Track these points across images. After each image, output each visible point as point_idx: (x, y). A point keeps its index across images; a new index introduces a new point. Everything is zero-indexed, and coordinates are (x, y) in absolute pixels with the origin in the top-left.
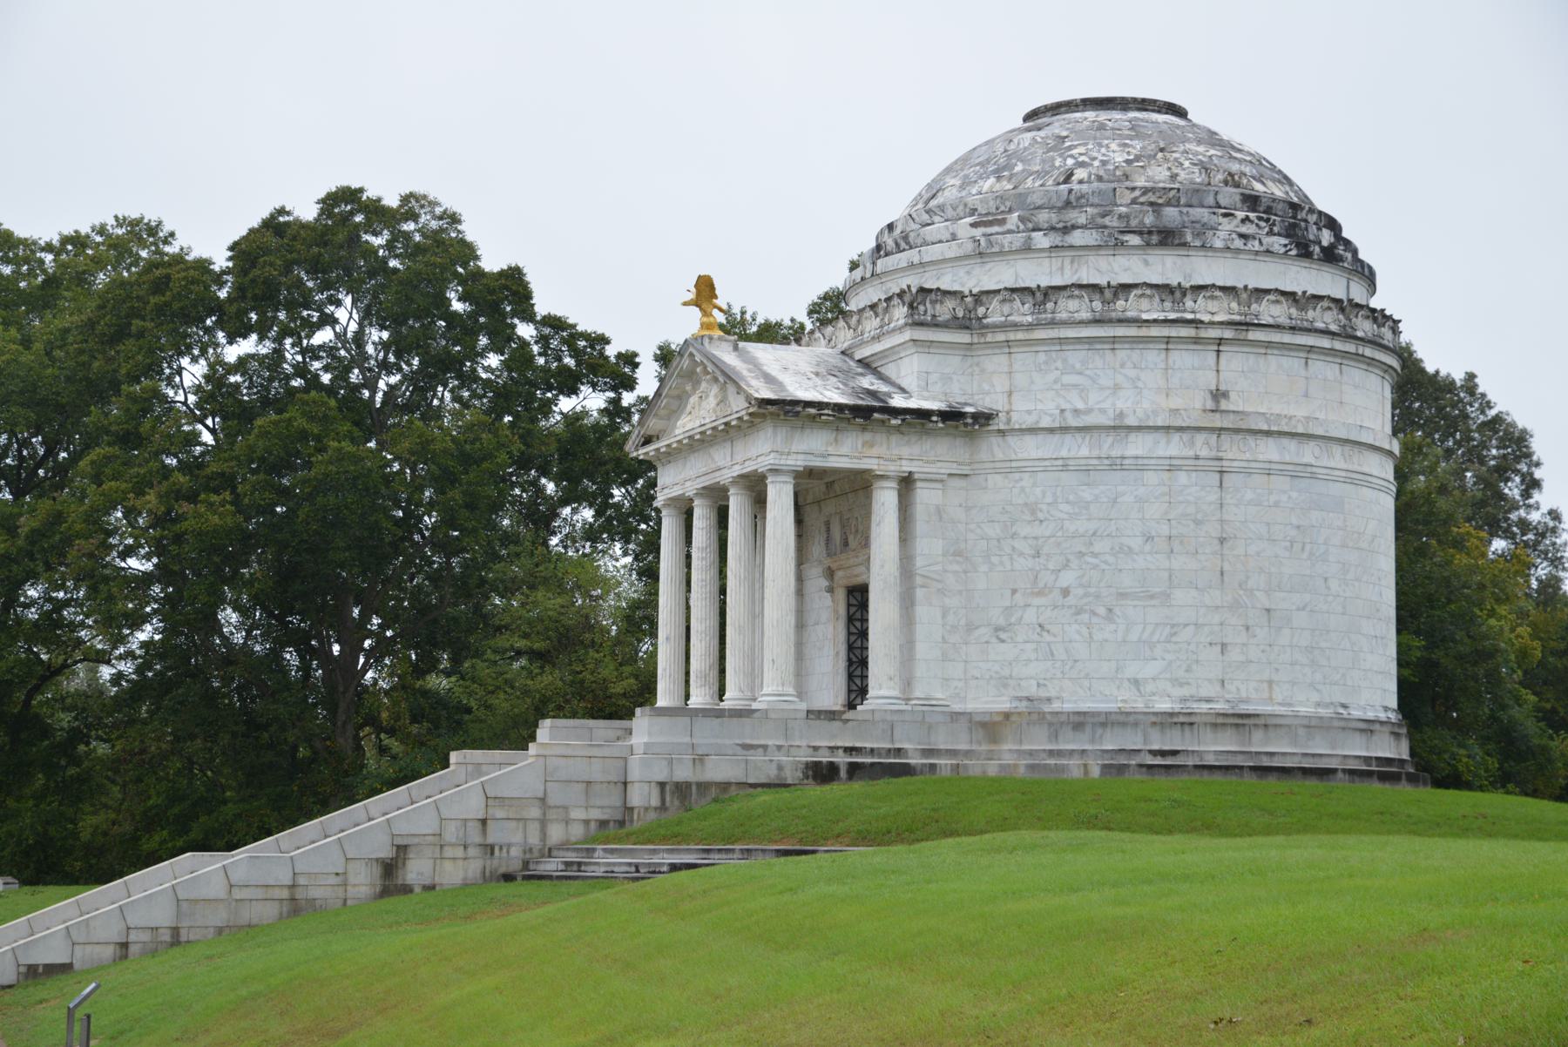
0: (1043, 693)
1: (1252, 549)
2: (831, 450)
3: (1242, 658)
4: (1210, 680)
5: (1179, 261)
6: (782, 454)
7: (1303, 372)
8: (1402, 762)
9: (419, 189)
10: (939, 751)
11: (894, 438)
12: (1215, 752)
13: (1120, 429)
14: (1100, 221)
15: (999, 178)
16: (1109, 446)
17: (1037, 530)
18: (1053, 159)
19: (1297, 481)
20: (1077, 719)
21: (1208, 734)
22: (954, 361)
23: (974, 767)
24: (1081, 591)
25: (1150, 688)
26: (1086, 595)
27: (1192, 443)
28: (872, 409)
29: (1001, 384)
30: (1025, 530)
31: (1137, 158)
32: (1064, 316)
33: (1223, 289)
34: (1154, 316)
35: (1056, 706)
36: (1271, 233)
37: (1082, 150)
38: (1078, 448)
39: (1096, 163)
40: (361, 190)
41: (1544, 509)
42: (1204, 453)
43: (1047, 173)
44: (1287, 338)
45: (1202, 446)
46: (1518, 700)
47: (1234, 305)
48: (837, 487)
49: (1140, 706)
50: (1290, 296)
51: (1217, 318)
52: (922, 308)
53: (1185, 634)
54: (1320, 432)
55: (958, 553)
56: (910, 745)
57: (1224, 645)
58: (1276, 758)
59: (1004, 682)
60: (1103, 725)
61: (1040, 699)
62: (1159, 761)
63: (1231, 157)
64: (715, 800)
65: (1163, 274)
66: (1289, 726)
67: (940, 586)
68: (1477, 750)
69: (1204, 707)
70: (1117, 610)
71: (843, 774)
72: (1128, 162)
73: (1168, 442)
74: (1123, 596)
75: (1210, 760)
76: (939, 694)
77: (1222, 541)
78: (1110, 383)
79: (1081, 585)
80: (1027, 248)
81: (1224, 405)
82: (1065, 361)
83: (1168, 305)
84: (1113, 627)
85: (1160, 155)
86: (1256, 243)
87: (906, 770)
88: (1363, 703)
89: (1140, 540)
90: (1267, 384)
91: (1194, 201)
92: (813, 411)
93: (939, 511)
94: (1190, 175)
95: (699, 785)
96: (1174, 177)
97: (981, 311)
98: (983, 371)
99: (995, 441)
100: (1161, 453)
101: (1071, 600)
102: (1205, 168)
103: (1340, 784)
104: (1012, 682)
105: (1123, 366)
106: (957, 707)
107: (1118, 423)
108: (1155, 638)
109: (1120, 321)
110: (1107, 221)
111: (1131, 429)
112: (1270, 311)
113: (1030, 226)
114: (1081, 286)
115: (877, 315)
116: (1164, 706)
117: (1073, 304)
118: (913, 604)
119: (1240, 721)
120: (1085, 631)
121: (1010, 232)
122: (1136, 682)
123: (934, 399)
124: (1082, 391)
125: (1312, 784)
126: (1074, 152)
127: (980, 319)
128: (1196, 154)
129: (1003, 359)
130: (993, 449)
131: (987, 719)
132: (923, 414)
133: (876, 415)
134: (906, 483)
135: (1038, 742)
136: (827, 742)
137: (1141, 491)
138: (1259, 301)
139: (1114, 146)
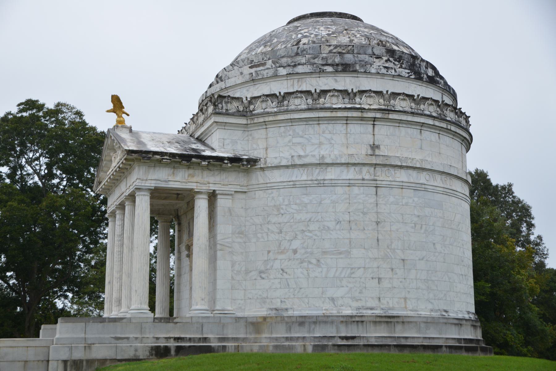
0: (284, 306)
1: (394, 228)
3: (390, 286)
4: (372, 298)
5: (353, 80)
6: (143, 180)
7: (419, 137)
8: (478, 341)
9: (62, 101)
10: (228, 338)
11: (206, 173)
13: (322, 165)
14: (312, 61)
15: (265, 46)
18: (292, 35)
19: (417, 192)
21: (372, 327)
22: (238, 134)
23: (247, 347)
24: (303, 251)
25: (340, 302)
26: (306, 253)
27: (361, 172)
28: (191, 156)
29: (262, 144)
30: (274, 219)
31: (333, 33)
32: (293, 107)
33: (375, 92)
34: (340, 106)
35: (290, 313)
36: (401, 67)
37: (306, 30)
38: (301, 176)
39: (312, 36)
40: (37, 101)
41: (536, 235)
42: (367, 177)
43: (288, 41)
44: (410, 118)
45: (366, 173)
46: (530, 309)
47: (381, 101)
49: (335, 312)
50: (411, 97)
51: (372, 107)
52: (220, 106)
53: (359, 273)
54: (429, 167)
55: (241, 233)
56: (212, 336)
57: (379, 279)
58: (409, 340)
60: (315, 323)
61: (282, 309)
62: (344, 342)
63: (381, 34)
65: (345, 86)
66: (416, 322)
67: (230, 250)
68: (515, 332)
69: (370, 312)
70: (322, 261)
71: (173, 352)
72: (328, 35)
73: (348, 172)
74: (324, 253)
75: (373, 342)
77: (378, 223)
78: (317, 141)
79: (303, 248)
80: (276, 76)
81: (377, 152)
82: (294, 131)
83: (347, 100)
84: (320, 270)
85: (345, 32)
86: (393, 71)
87: (209, 350)
88: (456, 309)
90: (401, 142)
91: (361, 52)
92: (158, 157)
94: (359, 40)
95: (88, 361)
96: (351, 41)
97: (252, 107)
98: (253, 138)
99: (259, 173)
100: (344, 177)
101: (298, 256)
102: (368, 38)
103: (445, 353)
104: (268, 301)
105: (324, 132)
106: (240, 314)
107: (321, 162)
108: (342, 276)
109: (321, 109)
110: (316, 61)
111: (328, 165)
112: (400, 104)
113: (278, 65)
114: (301, 92)
115: (203, 114)
116: (348, 312)
117: (297, 101)
119: (389, 320)
120: (305, 272)
121: (268, 69)
122: (333, 299)
123: (227, 152)
125: (429, 354)
126: (302, 32)
127: (251, 111)
128: (364, 32)
129: (263, 132)
130: (258, 178)
131: (255, 320)
132: (220, 159)
133: (193, 159)
134: (212, 197)
135: (281, 333)
136: (164, 335)
137: (334, 197)
138: (394, 99)
139: (322, 28)
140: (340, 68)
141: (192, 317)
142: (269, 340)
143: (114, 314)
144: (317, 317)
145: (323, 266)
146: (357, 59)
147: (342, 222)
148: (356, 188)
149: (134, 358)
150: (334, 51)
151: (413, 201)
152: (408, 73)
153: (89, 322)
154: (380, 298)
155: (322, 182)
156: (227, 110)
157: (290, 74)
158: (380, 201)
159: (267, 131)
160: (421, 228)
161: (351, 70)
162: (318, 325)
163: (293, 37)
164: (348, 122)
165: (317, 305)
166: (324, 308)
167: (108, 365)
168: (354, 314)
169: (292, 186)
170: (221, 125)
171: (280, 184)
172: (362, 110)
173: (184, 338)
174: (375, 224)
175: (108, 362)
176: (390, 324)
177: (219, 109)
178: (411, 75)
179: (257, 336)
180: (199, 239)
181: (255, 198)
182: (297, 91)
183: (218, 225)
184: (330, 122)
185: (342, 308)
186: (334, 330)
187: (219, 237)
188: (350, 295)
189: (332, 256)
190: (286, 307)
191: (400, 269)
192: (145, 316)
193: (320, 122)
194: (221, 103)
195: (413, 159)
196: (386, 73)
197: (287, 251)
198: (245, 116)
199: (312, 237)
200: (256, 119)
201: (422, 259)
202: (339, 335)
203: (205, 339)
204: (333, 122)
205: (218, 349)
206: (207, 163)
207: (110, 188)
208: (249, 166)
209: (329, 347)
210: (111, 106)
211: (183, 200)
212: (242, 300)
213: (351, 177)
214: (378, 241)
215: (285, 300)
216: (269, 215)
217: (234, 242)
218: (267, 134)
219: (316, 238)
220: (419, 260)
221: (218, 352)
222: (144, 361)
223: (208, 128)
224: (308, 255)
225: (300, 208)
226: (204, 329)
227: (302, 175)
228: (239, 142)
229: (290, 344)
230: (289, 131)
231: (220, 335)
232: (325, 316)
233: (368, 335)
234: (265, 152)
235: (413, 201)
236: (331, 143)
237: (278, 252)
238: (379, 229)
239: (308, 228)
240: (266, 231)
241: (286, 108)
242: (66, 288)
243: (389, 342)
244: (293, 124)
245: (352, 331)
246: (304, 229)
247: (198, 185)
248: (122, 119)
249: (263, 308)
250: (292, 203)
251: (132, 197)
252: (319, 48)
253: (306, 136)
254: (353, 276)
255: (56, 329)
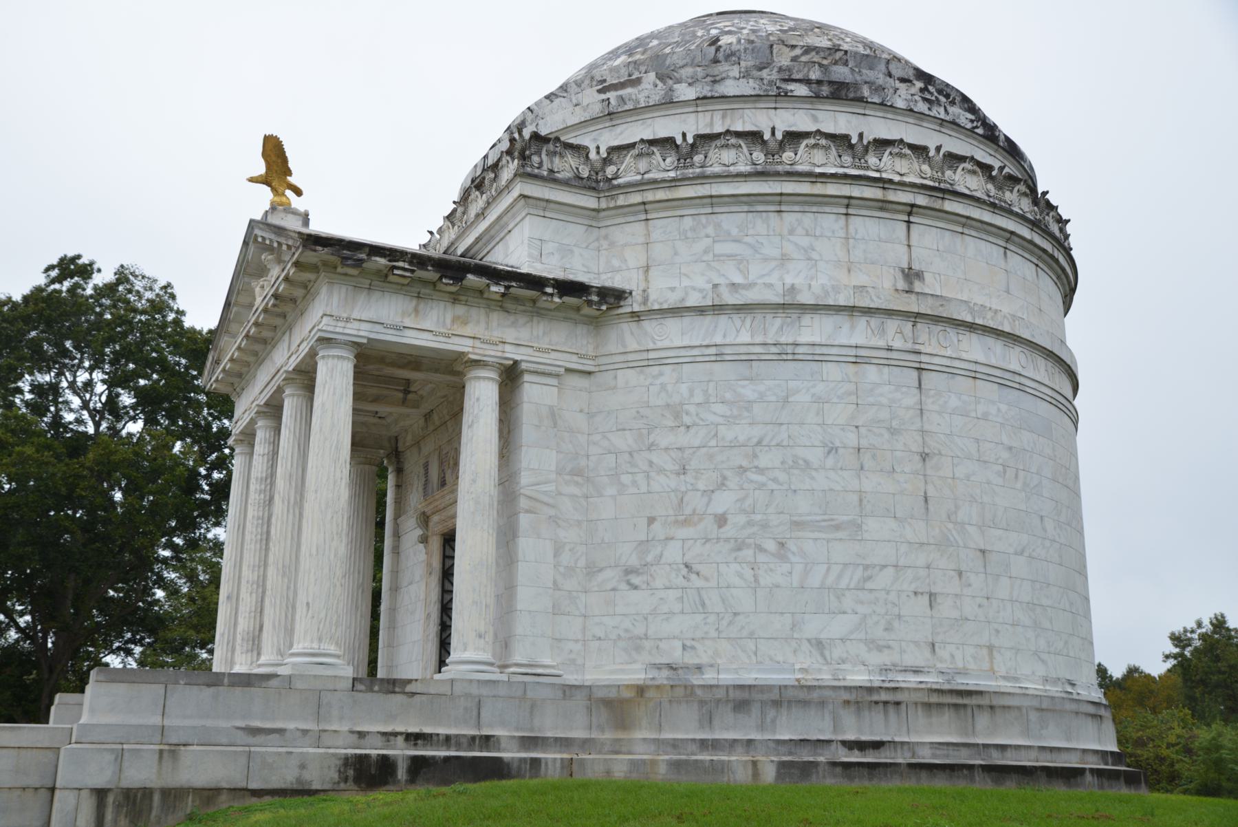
0: (690, 659)
2: (408, 322)
3: (955, 614)
4: (916, 643)
6: (338, 319)
7: (1002, 263)
10: (545, 739)
11: (496, 317)
12: (932, 745)
13: (791, 308)
16: (775, 329)
17: (683, 439)
20: (739, 695)
21: (920, 718)
22: (575, 232)
23: (595, 764)
24: (742, 519)
25: (838, 652)
26: (750, 523)
27: (882, 331)
29: (635, 258)
32: (717, 169)
34: (833, 171)
35: (709, 677)
39: (745, 31)
40: (79, 257)
42: (898, 344)
44: (987, 216)
45: (895, 334)
47: (925, 168)
48: (435, 417)
49: (826, 677)
51: (907, 179)
52: (535, 159)
53: (884, 579)
54: (1026, 335)
56: (505, 733)
57: (932, 595)
58: (1009, 754)
59: (635, 644)
60: (777, 704)
62: (855, 757)
64: (190, 818)
66: (1019, 708)
67: (552, 512)
69: (912, 680)
70: (791, 545)
71: (402, 773)
73: (853, 327)
74: (797, 525)
75: (926, 757)
76: (547, 660)
77: (924, 457)
78: (776, 253)
80: (669, 103)
81: (918, 286)
82: (718, 226)
84: (786, 567)
86: (942, 110)
87: (496, 770)
89: (820, 452)
92: (382, 261)
93: (553, 414)
95: (166, 793)
97: (610, 171)
98: (612, 244)
100: (844, 341)
101: (728, 531)
105: (792, 232)
106: (571, 678)
107: (788, 300)
108: (843, 584)
109: (789, 174)
110: (764, 73)
111: (804, 308)
116: (858, 677)
117: (728, 156)
118: (515, 535)
119: (959, 701)
120: (748, 573)
122: (819, 644)
124: (741, 262)
129: (639, 228)
130: (625, 337)
131: (613, 694)
132: (535, 282)
133: (470, 276)
134: (510, 376)
135: (684, 727)
136: (377, 725)
137: (820, 388)
140: (825, 90)
141: (452, 680)
142: (653, 748)
143: (241, 666)
144: (782, 688)
145: (793, 559)
146: (858, 78)
147: (841, 451)
148: (873, 368)
149: (295, 787)
150: (804, 59)
151: (999, 410)
152: (972, 121)
153: (177, 683)
154: (933, 645)
155: (789, 349)
156: (551, 171)
157: (705, 98)
158: (929, 404)
159: (647, 226)
160: (1017, 476)
161: (851, 95)
162: (784, 711)
163: (699, 34)
164: (851, 211)
165: (780, 658)
166: (797, 667)
167: (224, 806)
168: (876, 684)
169: (713, 358)
170: (536, 207)
171: (683, 352)
172: (884, 183)
173: (431, 735)
174: (918, 458)
175: (223, 797)
176: (962, 711)
177: (532, 166)
178: (977, 127)
179: (620, 735)
180: (474, 481)
181: (615, 388)
182: (728, 132)
183: (524, 449)
184: (807, 208)
185: (843, 666)
186: (827, 723)
187: (525, 479)
188: (862, 636)
189: (816, 535)
190: (697, 661)
191: (977, 573)
192: (329, 672)
193: (783, 208)
194: (539, 153)
195: (996, 312)
196: (927, 112)
197: (700, 520)
198: (594, 189)
199: (764, 485)
200: (621, 197)
201: (1021, 553)
202: (840, 738)
203: (487, 741)
204: (815, 209)
205: (519, 768)
206: (502, 290)
207: (245, 370)
208: (604, 308)
209: (820, 769)
210: (260, 168)
211: (418, 407)
212: (577, 641)
213: (860, 342)
214: (926, 500)
215: (693, 643)
216: (651, 429)
217: (560, 494)
218: (648, 235)
219: (775, 486)
220: (1016, 554)
221: (519, 775)
222: (322, 796)
223: (499, 218)
224: (755, 529)
225: (735, 412)
226: (483, 715)
227: (738, 331)
228: (576, 250)
229: (715, 758)
230: (705, 227)
231: (522, 729)
232: (802, 687)
233: (914, 739)
234: (642, 277)
235: (999, 410)
236: (809, 259)
237: (676, 522)
238: (929, 472)
239: (756, 463)
240: (645, 467)
241: (698, 170)
242: (129, 635)
243: (963, 758)
244: (716, 210)
245: (873, 728)
246: (745, 464)
247: (478, 343)
248: (284, 199)
249: (635, 662)
250: (712, 399)
251: (305, 377)
252: (768, 51)
253: (747, 239)
254: (869, 585)
255: (81, 704)
